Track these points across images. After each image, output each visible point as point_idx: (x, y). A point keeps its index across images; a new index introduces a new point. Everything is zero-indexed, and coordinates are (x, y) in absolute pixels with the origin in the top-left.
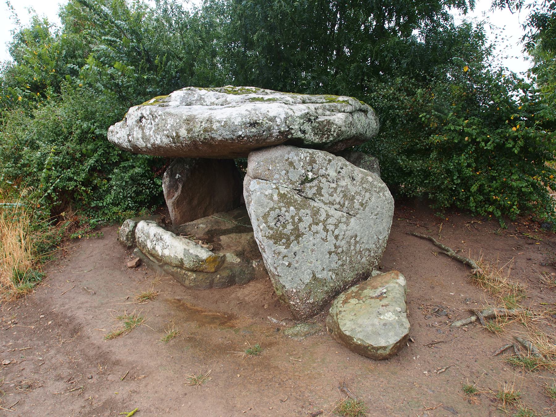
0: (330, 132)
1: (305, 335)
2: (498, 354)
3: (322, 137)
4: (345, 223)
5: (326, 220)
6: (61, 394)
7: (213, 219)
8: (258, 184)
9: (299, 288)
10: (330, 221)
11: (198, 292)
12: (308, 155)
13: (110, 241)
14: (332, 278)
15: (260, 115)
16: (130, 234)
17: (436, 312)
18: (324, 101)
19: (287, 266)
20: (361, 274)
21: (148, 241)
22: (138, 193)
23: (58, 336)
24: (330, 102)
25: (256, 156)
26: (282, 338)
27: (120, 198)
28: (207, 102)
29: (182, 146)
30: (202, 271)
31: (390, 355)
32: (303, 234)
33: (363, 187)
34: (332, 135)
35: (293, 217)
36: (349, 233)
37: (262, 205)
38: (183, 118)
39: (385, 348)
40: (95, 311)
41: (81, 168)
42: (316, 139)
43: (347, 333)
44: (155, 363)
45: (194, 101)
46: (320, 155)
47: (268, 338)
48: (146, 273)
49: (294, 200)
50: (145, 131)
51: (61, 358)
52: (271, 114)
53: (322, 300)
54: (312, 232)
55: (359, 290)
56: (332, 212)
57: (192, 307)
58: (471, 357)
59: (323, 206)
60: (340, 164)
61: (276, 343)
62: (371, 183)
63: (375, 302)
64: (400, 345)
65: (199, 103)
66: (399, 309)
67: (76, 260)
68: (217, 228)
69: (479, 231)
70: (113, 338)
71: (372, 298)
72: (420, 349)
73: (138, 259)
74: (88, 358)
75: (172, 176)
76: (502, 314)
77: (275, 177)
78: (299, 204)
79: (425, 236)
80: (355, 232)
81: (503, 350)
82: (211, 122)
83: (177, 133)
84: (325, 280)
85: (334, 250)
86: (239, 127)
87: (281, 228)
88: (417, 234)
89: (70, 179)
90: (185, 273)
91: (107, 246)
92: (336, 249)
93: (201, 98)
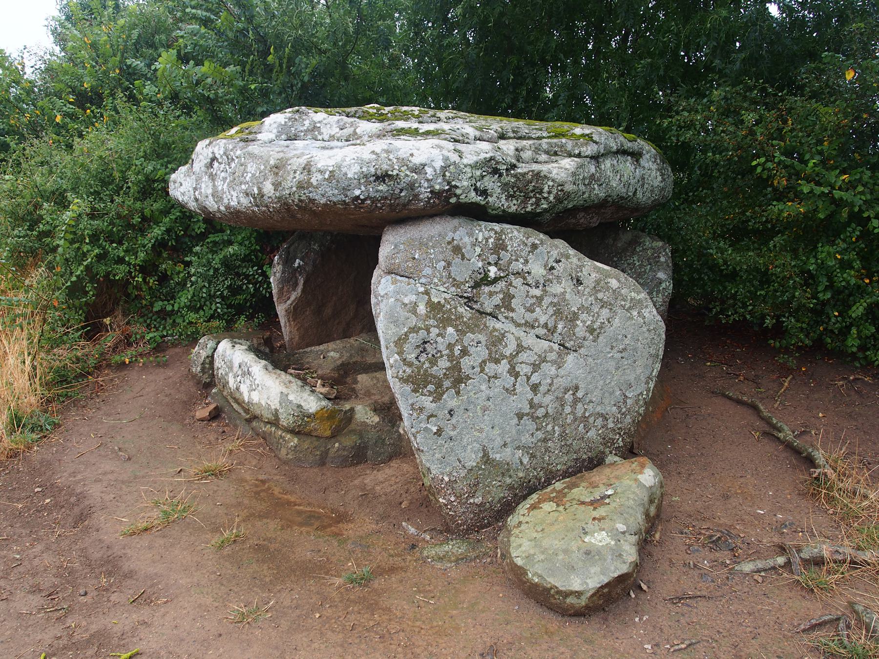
0: (541, 192)
1: (457, 561)
2: (804, 631)
4: (554, 362)
5: (515, 356)
6: (31, 614)
7: (356, 344)
8: (392, 284)
9: (455, 474)
10: (523, 356)
11: (299, 471)
12: (492, 234)
13: (173, 374)
14: (521, 463)
15: (395, 161)
16: (207, 361)
17: (714, 541)
19: (435, 433)
20: (584, 460)
21: (230, 375)
22: (235, 290)
23: (54, 523)
24: (556, 136)
25: (394, 234)
26: (415, 561)
27: (202, 297)
28: (325, 134)
29: (269, 211)
30: (309, 434)
31: (587, 607)
32: (468, 378)
33: (596, 299)
34: (544, 198)
35: (450, 346)
37: (395, 322)
39: (578, 594)
40: (121, 489)
41: (139, 242)
42: (513, 207)
43: (519, 562)
44: (188, 580)
45: (302, 131)
46: (515, 235)
47: (391, 559)
48: (224, 432)
49: (455, 315)
51: (48, 559)
52: (417, 160)
53: (499, 501)
54: (486, 375)
55: (565, 488)
56: (529, 340)
57: (280, 496)
58: (749, 629)
59: (513, 329)
60: (555, 253)
61: (402, 568)
62: (614, 291)
63: (583, 512)
64: (609, 592)
65: (309, 137)
66: (621, 527)
67: (113, 401)
68: (358, 359)
70: (134, 533)
71: (583, 503)
72: (654, 604)
73: (212, 407)
74: (88, 563)
75: (287, 262)
76: (840, 557)
77: (424, 273)
78: (465, 323)
79: (745, 398)
80: (575, 381)
81: (816, 625)
83: (260, 189)
84: (508, 464)
85: (527, 411)
86: (355, 181)
87: (427, 365)
88: (731, 394)
89: (120, 261)
90: (281, 436)
91: (170, 380)
92: (533, 410)
93: (315, 127)
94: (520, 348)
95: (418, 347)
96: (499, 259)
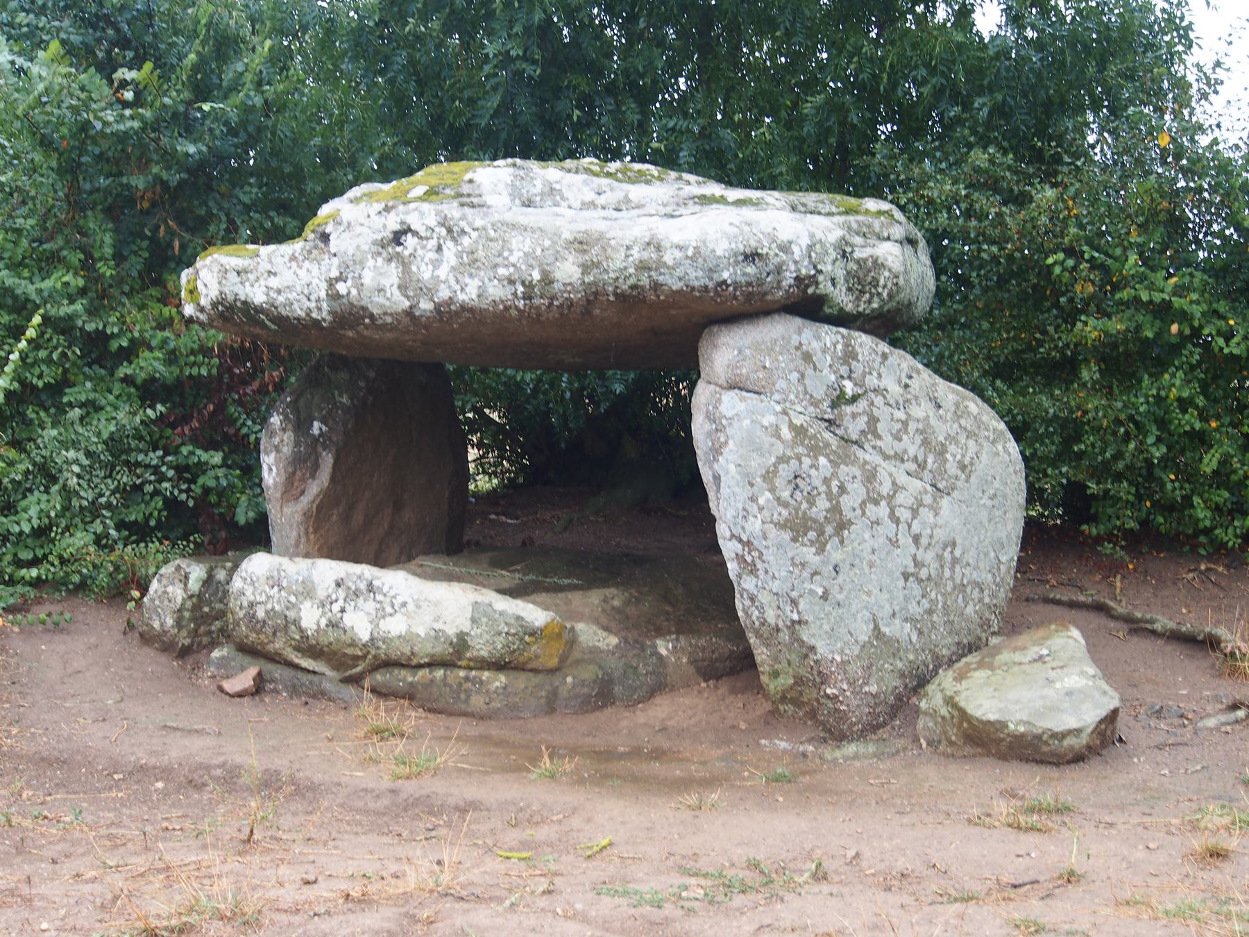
0: (876, 286)
3: (858, 299)
12: (839, 337)
16: (189, 604)
18: (834, 209)
31: (1089, 747)
32: (850, 523)
35: (827, 481)
36: (940, 535)
37: (759, 450)
38: (563, 236)
39: (1077, 732)
46: (864, 342)
50: (414, 268)
52: (783, 236)
53: (892, 693)
56: (902, 479)
69: (1222, 589)
78: (835, 452)
82: (658, 248)
86: (725, 261)
88: (1058, 597)
94: (896, 487)
95: (790, 482)
96: (851, 371)
